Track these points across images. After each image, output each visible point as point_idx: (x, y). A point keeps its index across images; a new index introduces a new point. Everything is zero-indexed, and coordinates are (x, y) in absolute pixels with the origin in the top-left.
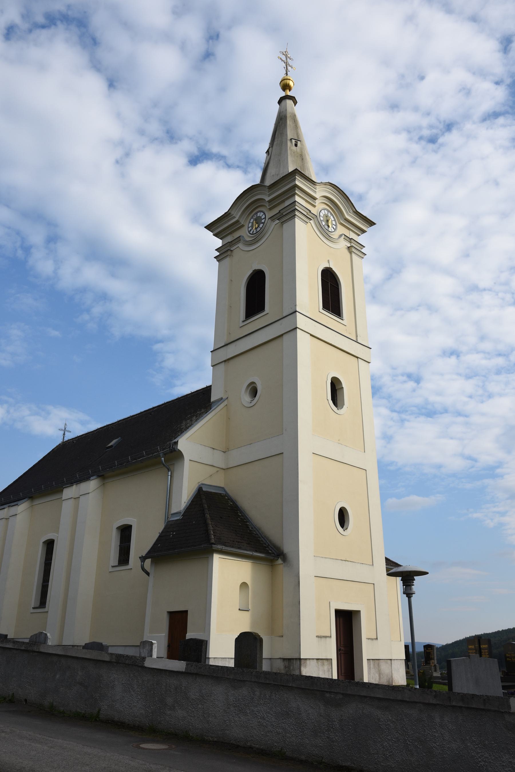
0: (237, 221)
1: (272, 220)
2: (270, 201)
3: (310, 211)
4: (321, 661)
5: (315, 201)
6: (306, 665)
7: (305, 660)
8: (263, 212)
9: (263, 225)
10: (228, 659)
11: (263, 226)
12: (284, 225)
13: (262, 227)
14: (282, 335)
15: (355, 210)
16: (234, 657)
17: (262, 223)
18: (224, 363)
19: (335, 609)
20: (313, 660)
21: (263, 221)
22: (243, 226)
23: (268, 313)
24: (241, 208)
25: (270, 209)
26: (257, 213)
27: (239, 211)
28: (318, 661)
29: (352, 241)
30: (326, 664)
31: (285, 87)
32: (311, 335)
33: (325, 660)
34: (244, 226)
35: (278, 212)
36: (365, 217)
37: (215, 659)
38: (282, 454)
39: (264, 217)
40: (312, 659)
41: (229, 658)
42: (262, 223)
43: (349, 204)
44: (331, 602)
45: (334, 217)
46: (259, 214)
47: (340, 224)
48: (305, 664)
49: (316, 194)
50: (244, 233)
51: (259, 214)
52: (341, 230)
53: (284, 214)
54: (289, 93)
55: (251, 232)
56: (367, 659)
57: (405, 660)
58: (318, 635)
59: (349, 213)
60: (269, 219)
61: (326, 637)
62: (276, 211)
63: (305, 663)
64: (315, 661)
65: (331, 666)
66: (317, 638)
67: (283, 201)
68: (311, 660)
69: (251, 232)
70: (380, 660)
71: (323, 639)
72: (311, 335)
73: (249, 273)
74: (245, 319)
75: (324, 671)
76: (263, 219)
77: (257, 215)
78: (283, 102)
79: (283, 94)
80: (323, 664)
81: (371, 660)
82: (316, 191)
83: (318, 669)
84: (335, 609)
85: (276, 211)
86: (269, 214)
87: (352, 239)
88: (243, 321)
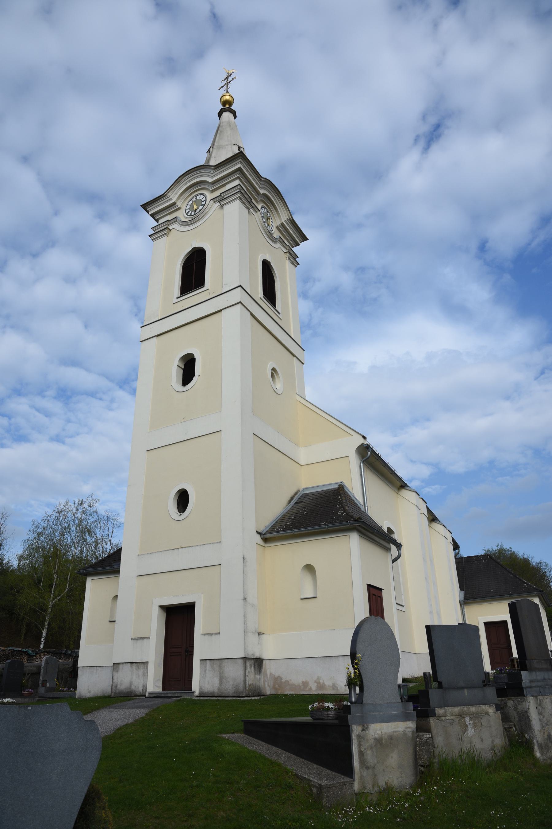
0: (174, 204)
1: (214, 202)
2: (214, 183)
4: (136, 665)
6: (118, 669)
7: (118, 664)
8: (203, 195)
9: (202, 207)
10: (95, 668)
11: (202, 208)
12: (225, 207)
13: (201, 210)
14: (221, 311)
15: (213, 167)
17: (202, 205)
18: (156, 337)
20: (126, 664)
21: (203, 203)
22: (179, 208)
23: (209, 289)
24: (178, 191)
25: (213, 191)
26: (196, 196)
27: (176, 195)
28: (132, 665)
30: (142, 667)
33: (140, 664)
34: (181, 209)
35: (220, 194)
36: (227, 159)
37: (84, 668)
38: (220, 432)
39: (204, 199)
41: (97, 666)
42: (202, 205)
46: (198, 197)
48: (117, 668)
50: (181, 215)
51: (198, 197)
53: (225, 197)
55: (189, 214)
56: (200, 660)
58: (135, 637)
59: (212, 175)
60: (211, 200)
62: (217, 193)
63: (117, 667)
64: (129, 665)
66: (133, 640)
67: (224, 185)
68: (124, 664)
69: (189, 214)
70: (223, 660)
71: (139, 642)
73: (197, 245)
74: (180, 295)
75: (139, 676)
76: (203, 202)
77: (197, 198)
80: (138, 668)
81: (208, 661)
82: (171, 197)
83: (132, 674)
85: (217, 193)
86: (210, 196)
88: (178, 298)
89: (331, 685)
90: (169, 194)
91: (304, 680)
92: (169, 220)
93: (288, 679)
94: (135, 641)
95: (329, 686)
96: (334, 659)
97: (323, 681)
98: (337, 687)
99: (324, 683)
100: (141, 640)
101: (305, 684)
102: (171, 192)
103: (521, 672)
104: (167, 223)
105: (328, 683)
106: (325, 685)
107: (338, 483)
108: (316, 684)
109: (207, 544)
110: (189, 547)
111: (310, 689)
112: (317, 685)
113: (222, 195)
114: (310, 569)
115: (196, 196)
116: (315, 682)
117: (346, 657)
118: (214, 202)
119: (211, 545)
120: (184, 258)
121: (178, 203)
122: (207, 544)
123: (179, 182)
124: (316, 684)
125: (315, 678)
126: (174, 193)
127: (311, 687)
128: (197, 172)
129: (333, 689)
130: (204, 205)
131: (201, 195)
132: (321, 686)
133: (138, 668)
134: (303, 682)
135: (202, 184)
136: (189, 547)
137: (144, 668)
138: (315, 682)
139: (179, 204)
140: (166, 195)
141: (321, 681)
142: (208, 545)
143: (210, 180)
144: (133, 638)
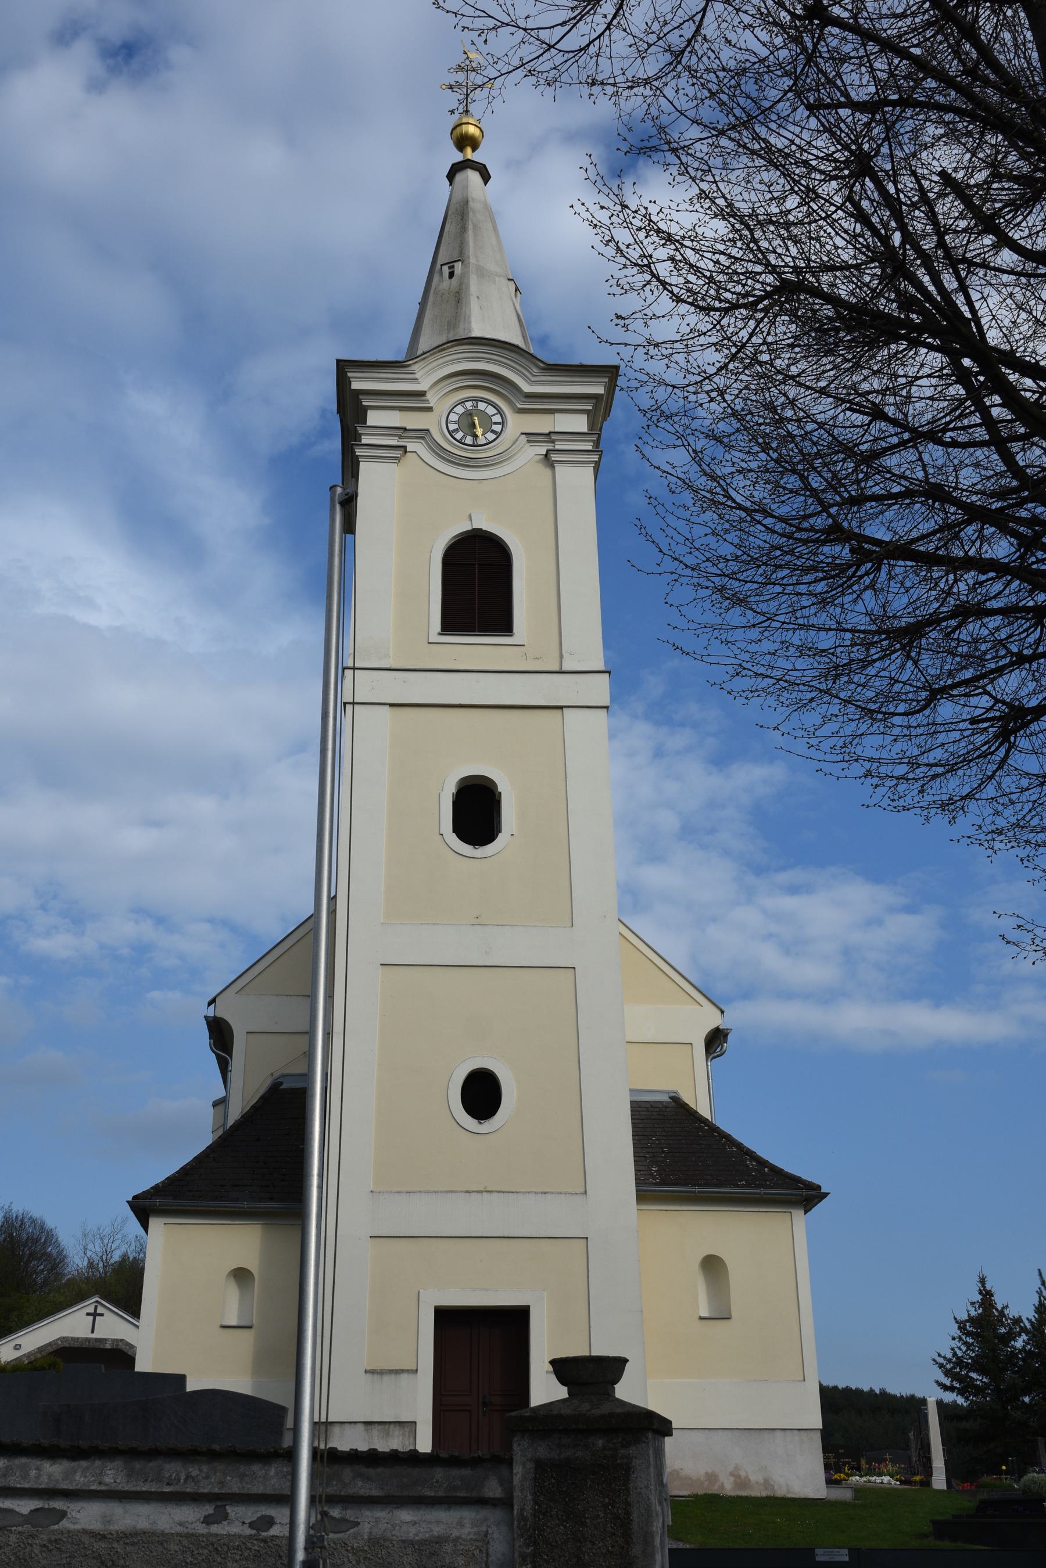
0: (421, 394)
3: (405, 429)
4: (380, 1427)
5: (424, 398)
15: (541, 365)
16: (593, 1354)
19: (435, 1307)
20: (352, 1425)
22: (430, 409)
29: (554, 437)
30: (397, 1433)
31: (464, 142)
32: (392, 705)
33: (392, 1426)
36: (581, 366)
40: (350, 1423)
43: (525, 358)
44: (421, 1291)
45: (495, 406)
47: (518, 413)
49: (419, 383)
51: (482, 406)
52: (516, 424)
54: (469, 154)
57: (416, 1451)
59: (533, 379)
61: (408, 1371)
64: (361, 1427)
65: (412, 1439)
66: (369, 1376)
68: (347, 1425)
72: (392, 705)
78: (459, 177)
79: (458, 157)
82: (417, 376)
84: (435, 1307)
87: (550, 433)
89: (762, 1481)
90: (415, 367)
91: (710, 1471)
92: (408, 428)
93: (676, 1467)
94: (376, 1377)
95: (757, 1483)
96: (766, 1434)
97: (747, 1473)
98: (773, 1486)
99: (747, 1477)
100: (393, 1376)
101: (712, 1477)
102: (421, 363)
103: (188, 1390)
104: (399, 432)
105: (755, 1477)
106: (749, 1480)
107: (668, 1092)
108: (732, 1479)
109: (553, 1193)
110: (509, 1192)
111: (722, 1486)
112: (735, 1481)
113: (552, 435)
114: (712, 1265)
115: (477, 400)
116: (732, 1474)
117: (788, 1431)
118: (529, 441)
119: (563, 1196)
120: (452, 539)
121: (429, 396)
122: (553, 1193)
123: (444, 349)
124: (732, 1479)
125: (731, 1468)
126: (427, 369)
127: (723, 1484)
128: (504, 351)
129: (766, 1489)
130: (498, 435)
131: (489, 404)
132: (742, 1482)
133: (388, 1434)
134: (707, 1473)
135: (499, 382)
136: (509, 1192)
137: (404, 1435)
138: (732, 1474)
139: (432, 399)
140: (409, 366)
141: (742, 1474)
142: (554, 1195)
143: (527, 388)
144: (368, 1369)
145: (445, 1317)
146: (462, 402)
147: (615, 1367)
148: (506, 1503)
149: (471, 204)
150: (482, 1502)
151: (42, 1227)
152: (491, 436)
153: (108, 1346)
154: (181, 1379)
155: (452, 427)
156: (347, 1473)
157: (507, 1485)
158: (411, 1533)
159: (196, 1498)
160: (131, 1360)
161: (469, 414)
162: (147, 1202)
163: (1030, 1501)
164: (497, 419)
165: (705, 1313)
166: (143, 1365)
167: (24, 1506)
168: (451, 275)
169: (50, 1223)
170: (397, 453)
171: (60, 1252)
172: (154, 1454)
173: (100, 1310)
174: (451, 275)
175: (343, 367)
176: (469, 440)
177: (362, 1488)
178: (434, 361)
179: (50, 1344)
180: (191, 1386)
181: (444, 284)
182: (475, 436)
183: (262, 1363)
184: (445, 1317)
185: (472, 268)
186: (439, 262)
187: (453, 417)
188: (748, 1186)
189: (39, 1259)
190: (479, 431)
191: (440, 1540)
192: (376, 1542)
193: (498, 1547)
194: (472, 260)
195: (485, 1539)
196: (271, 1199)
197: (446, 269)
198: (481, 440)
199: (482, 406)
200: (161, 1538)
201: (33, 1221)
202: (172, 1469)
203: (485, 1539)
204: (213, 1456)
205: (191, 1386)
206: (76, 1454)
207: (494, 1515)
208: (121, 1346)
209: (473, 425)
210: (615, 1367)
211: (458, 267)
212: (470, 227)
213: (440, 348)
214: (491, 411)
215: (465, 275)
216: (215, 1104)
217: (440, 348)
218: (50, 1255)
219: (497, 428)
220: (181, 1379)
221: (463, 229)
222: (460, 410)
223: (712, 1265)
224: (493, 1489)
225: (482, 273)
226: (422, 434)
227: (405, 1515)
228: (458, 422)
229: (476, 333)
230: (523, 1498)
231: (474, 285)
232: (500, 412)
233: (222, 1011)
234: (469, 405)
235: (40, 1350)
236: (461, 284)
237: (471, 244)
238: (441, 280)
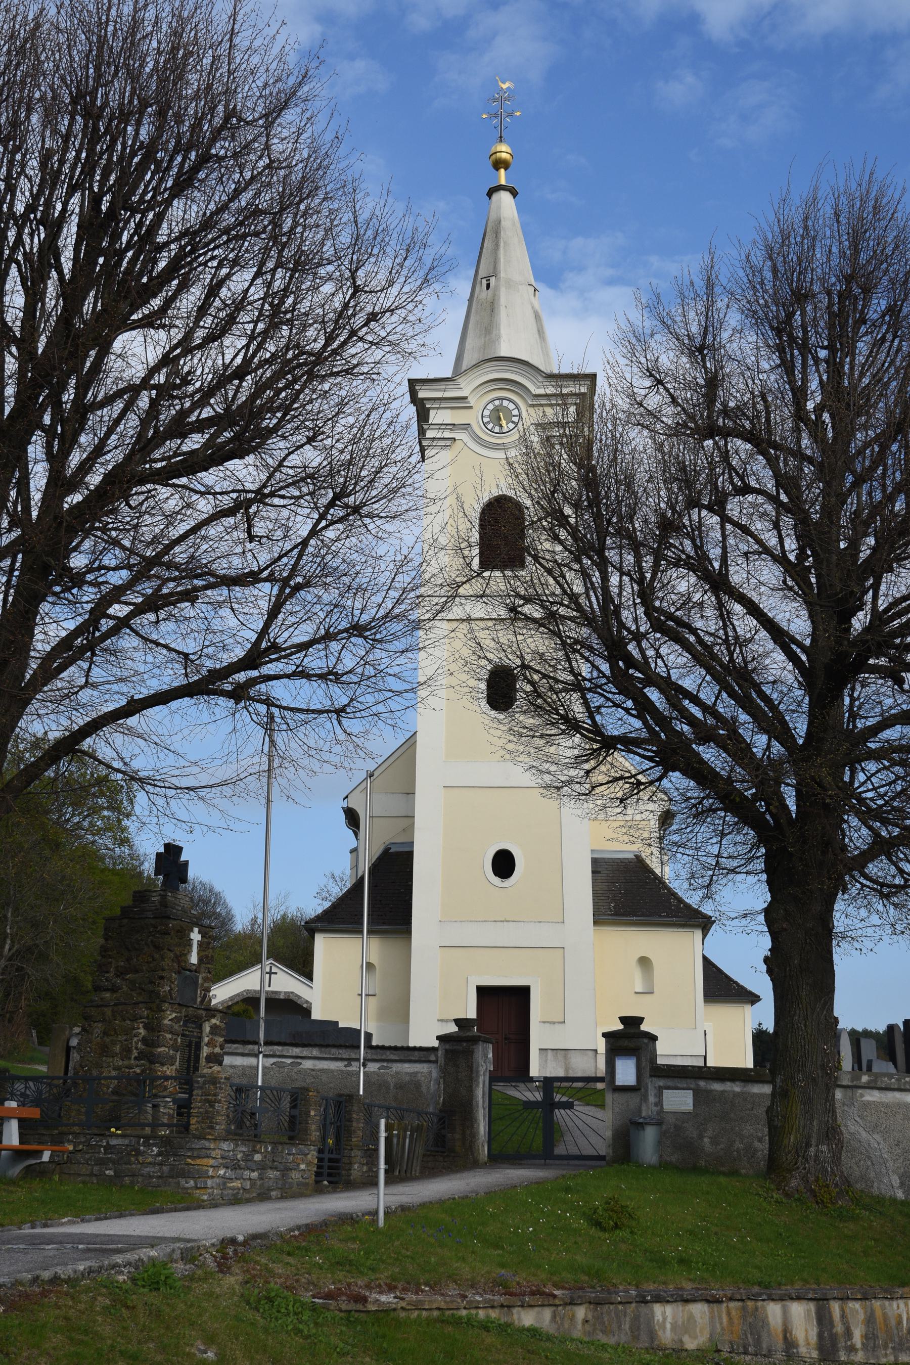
0: (464, 398)
22: (471, 407)
51: (505, 403)
78: (495, 196)
114: (644, 962)
115: (502, 399)
121: (469, 399)
139: (472, 401)
145: (482, 991)
146: (492, 401)
147: (641, 1020)
148: (436, 1062)
149: (503, 223)
150: (430, 1062)
151: (211, 891)
152: (511, 426)
153: (282, 997)
154: (337, 1023)
155: (486, 420)
156: (388, 1053)
157: (437, 1056)
158: (408, 1070)
159: (342, 1059)
160: (307, 1012)
161: (497, 410)
162: (313, 925)
163: (906, 1106)
164: (515, 412)
165: (639, 989)
166: (316, 1015)
167: (289, 1061)
168: (488, 286)
169: (218, 888)
170: (448, 443)
171: (229, 912)
172: (328, 1046)
173: (274, 970)
174: (488, 286)
175: (412, 383)
176: (497, 429)
177: (392, 1057)
178: (471, 375)
179: (238, 995)
180: (341, 1026)
181: (483, 294)
182: (501, 426)
183: (383, 1014)
184: (482, 991)
185: (502, 282)
186: (480, 276)
187: (487, 413)
188: (667, 916)
189: (209, 918)
190: (504, 422)
191: (417, 1073)
192: (397, 1073)
193: (435, 1074)
194: (502, 275)
195: (430, 1072)
196: (384, 923)
197: (484, 282)
198: (505, 429)
199: (505, 403)
200: (332, 1071)
201: (203, 885)
202: (334, 1050)
203: (430, 1072)
204: (346, 1047)
205: (341, 1026)
206: (304, 1046)
207: (433, 1066)
208: (292, 997)
209: (500, 419)
210: (641, 1020)
211: (493, 280)
212: (502, 245)
213: (476, 366)
214: (511, 406)
215: (497, 288)
216: (352, 851)
217: (476, 366)
218: (220, 914)
219: (515, 419)
220: (337, 1023)
221: (497, 246)
222: (491, 407)
223: (644, 962)
224: (433, 1058)
225: (510, 284)
226: (466, 427)
227: (406, 1065)
228: (490, 416)
229: (503, 353)
230: (441, 1060)
231: (504, 297)
232: (517, 407)
233: (355, 803)
234: (497, 403)
235: (231, 998)
236: (494, 295)
237: (502, 260)
238: (481, 291)
